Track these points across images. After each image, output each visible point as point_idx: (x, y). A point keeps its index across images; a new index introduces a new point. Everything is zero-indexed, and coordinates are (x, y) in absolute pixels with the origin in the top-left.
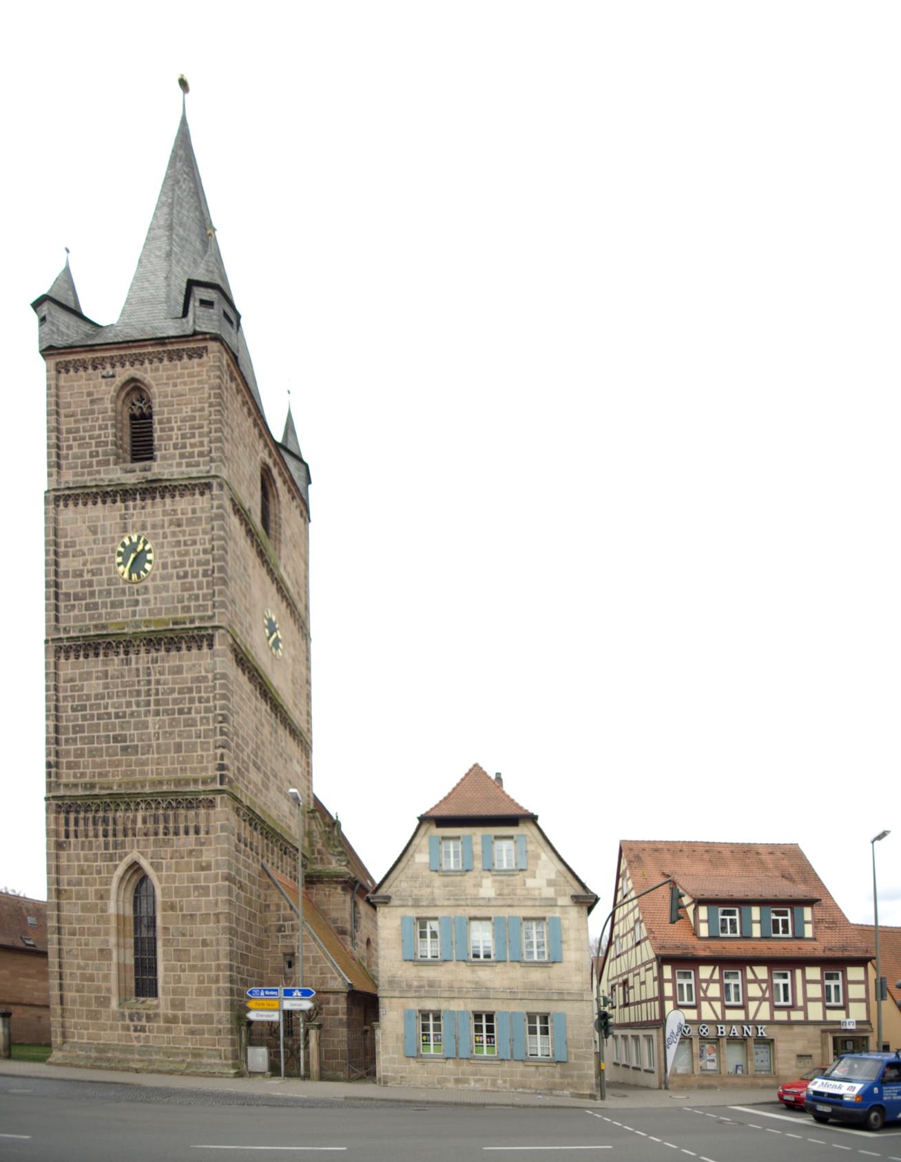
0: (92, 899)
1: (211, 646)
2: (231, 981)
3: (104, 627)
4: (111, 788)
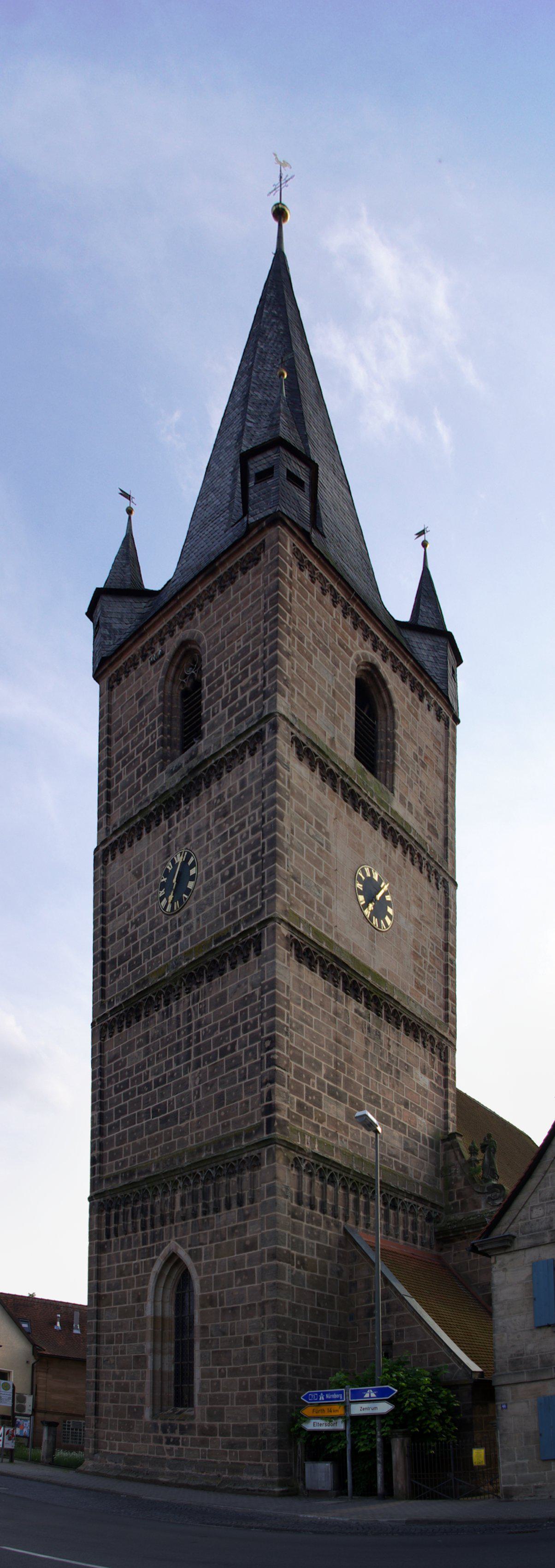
0: (130, 1303)
1: (258, 951)
2: (280, 1383)
3: (145, 981)
4: (149, 1171)
